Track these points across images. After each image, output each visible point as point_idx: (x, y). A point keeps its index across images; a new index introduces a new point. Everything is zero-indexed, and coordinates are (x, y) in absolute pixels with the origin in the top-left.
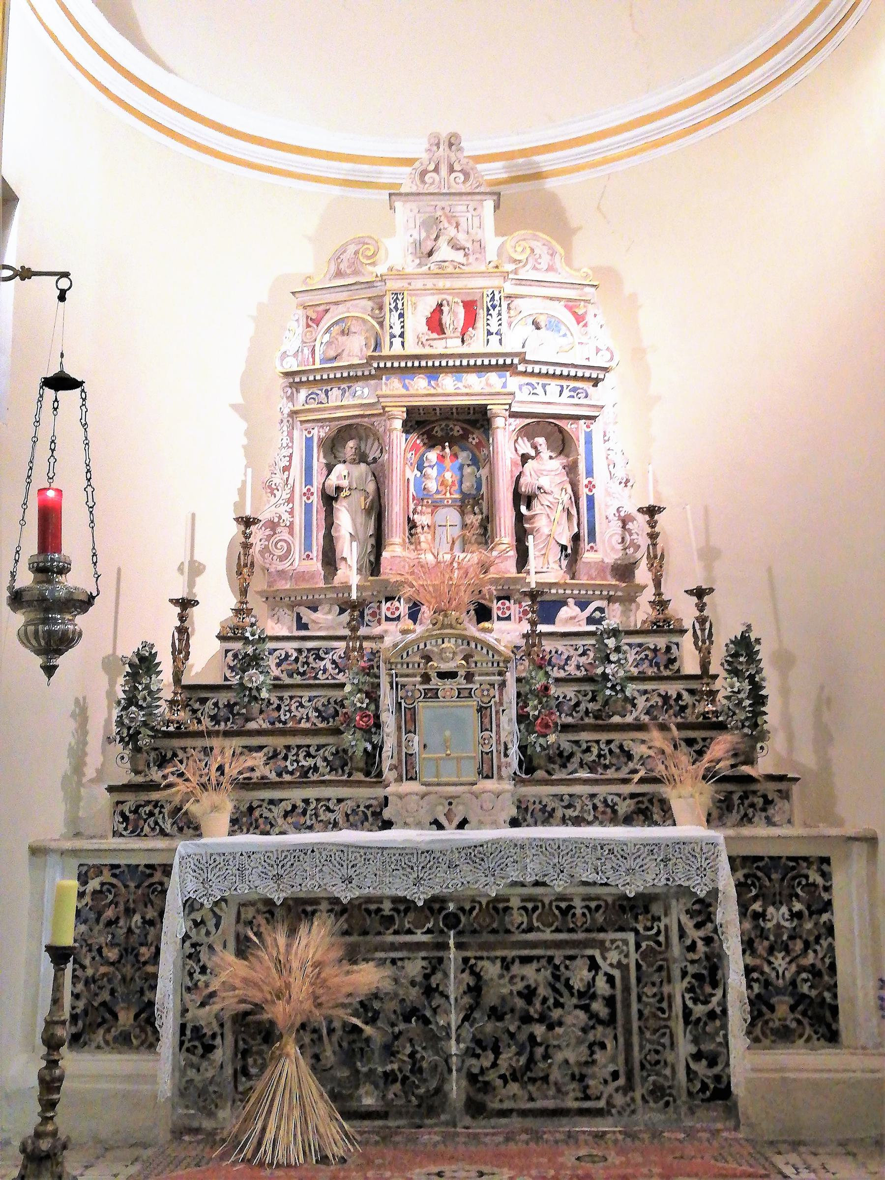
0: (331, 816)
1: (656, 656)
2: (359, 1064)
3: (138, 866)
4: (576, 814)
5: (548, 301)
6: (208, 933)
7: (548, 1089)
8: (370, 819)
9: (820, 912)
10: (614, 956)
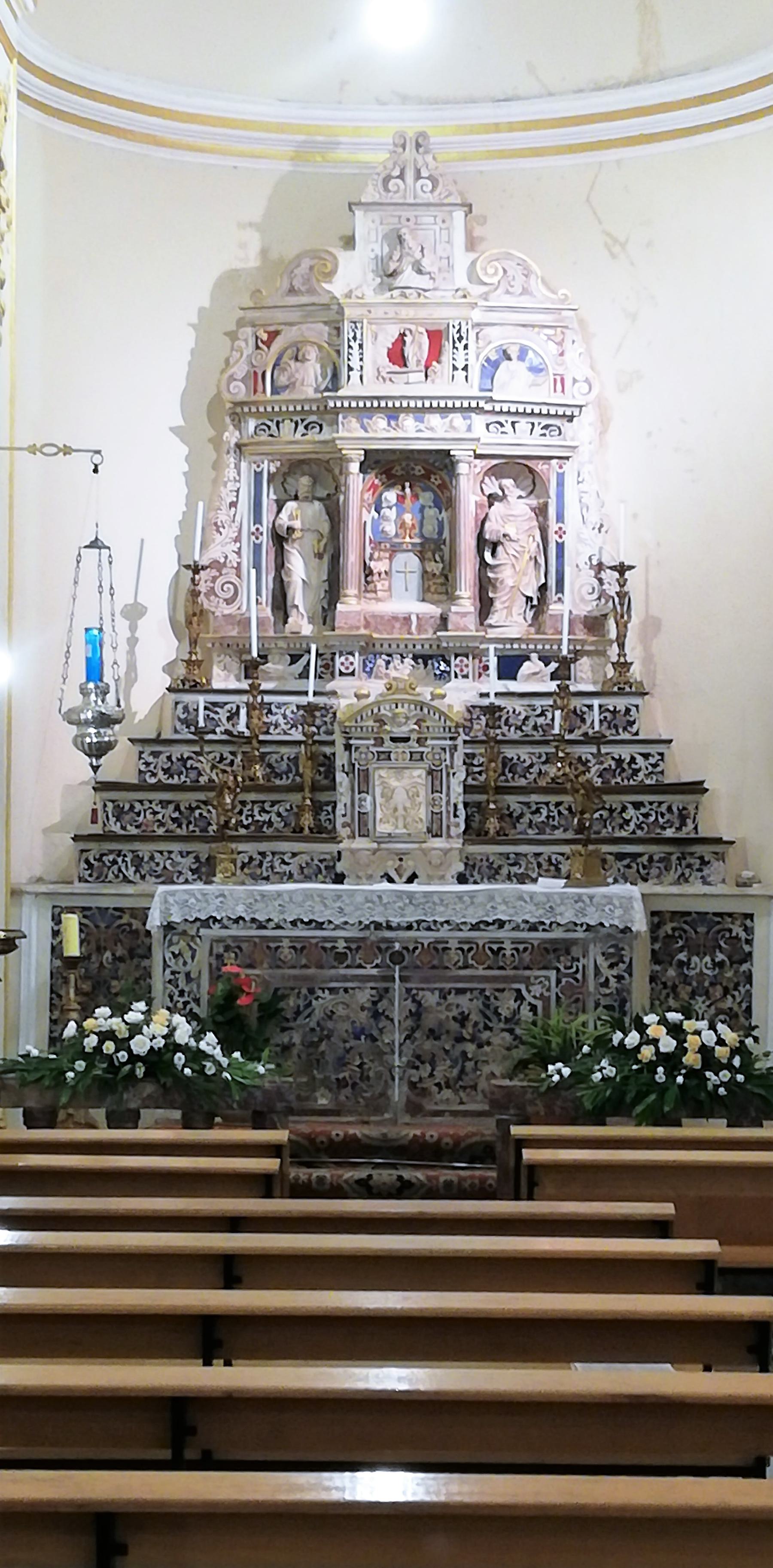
0: (286, 868)
1: (615, 718)
2: (315, 1072)
3: (107, 909)
4: (522, 870)
8: (324, 872)
9: (742, 962)
10: (537, 990)
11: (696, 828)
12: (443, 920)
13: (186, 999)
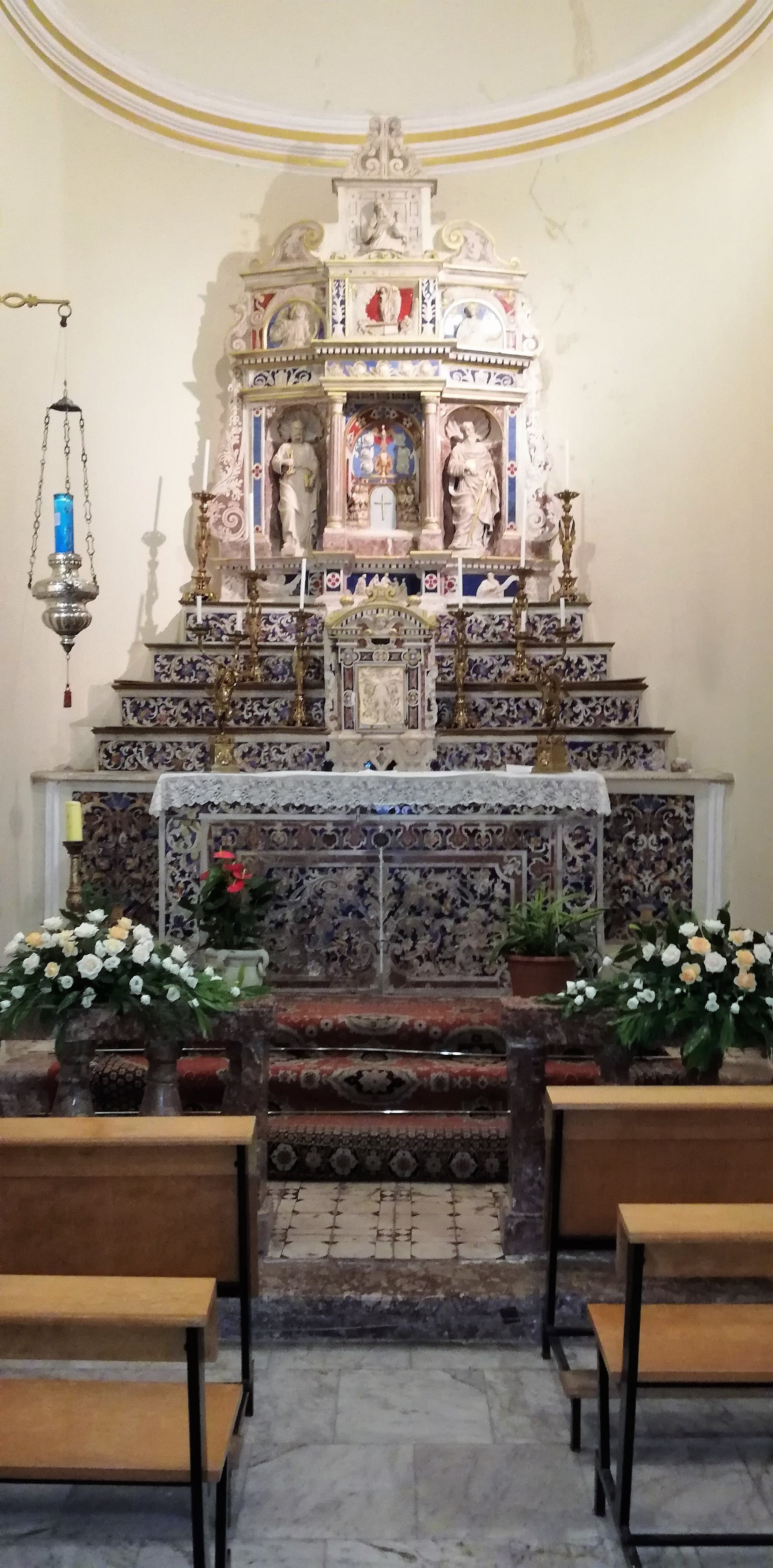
0: (282, 757)
2: (307, 946)
3: (122, 794)
5: (480, 290)
6: (186, 846)
7: (455, 967)
8: (314, 760)
9: (683, 839)
10: (510, 869)
11: (637, 720)
12: (423, 804)
13: (186, 879)
